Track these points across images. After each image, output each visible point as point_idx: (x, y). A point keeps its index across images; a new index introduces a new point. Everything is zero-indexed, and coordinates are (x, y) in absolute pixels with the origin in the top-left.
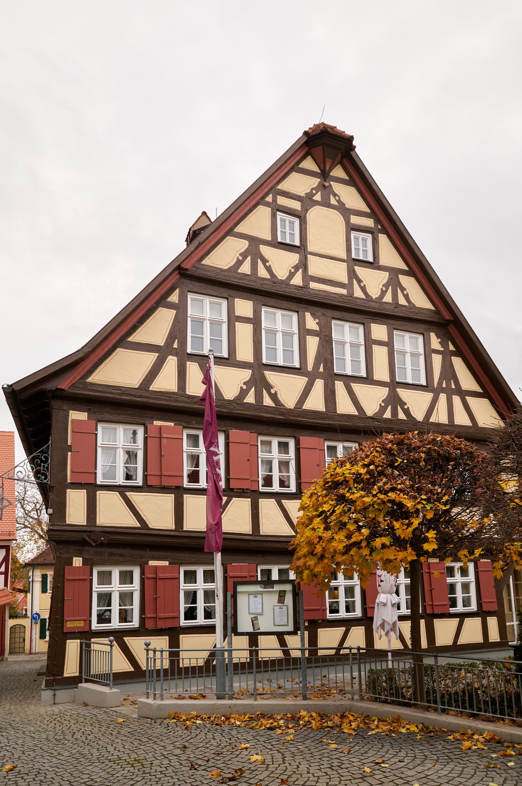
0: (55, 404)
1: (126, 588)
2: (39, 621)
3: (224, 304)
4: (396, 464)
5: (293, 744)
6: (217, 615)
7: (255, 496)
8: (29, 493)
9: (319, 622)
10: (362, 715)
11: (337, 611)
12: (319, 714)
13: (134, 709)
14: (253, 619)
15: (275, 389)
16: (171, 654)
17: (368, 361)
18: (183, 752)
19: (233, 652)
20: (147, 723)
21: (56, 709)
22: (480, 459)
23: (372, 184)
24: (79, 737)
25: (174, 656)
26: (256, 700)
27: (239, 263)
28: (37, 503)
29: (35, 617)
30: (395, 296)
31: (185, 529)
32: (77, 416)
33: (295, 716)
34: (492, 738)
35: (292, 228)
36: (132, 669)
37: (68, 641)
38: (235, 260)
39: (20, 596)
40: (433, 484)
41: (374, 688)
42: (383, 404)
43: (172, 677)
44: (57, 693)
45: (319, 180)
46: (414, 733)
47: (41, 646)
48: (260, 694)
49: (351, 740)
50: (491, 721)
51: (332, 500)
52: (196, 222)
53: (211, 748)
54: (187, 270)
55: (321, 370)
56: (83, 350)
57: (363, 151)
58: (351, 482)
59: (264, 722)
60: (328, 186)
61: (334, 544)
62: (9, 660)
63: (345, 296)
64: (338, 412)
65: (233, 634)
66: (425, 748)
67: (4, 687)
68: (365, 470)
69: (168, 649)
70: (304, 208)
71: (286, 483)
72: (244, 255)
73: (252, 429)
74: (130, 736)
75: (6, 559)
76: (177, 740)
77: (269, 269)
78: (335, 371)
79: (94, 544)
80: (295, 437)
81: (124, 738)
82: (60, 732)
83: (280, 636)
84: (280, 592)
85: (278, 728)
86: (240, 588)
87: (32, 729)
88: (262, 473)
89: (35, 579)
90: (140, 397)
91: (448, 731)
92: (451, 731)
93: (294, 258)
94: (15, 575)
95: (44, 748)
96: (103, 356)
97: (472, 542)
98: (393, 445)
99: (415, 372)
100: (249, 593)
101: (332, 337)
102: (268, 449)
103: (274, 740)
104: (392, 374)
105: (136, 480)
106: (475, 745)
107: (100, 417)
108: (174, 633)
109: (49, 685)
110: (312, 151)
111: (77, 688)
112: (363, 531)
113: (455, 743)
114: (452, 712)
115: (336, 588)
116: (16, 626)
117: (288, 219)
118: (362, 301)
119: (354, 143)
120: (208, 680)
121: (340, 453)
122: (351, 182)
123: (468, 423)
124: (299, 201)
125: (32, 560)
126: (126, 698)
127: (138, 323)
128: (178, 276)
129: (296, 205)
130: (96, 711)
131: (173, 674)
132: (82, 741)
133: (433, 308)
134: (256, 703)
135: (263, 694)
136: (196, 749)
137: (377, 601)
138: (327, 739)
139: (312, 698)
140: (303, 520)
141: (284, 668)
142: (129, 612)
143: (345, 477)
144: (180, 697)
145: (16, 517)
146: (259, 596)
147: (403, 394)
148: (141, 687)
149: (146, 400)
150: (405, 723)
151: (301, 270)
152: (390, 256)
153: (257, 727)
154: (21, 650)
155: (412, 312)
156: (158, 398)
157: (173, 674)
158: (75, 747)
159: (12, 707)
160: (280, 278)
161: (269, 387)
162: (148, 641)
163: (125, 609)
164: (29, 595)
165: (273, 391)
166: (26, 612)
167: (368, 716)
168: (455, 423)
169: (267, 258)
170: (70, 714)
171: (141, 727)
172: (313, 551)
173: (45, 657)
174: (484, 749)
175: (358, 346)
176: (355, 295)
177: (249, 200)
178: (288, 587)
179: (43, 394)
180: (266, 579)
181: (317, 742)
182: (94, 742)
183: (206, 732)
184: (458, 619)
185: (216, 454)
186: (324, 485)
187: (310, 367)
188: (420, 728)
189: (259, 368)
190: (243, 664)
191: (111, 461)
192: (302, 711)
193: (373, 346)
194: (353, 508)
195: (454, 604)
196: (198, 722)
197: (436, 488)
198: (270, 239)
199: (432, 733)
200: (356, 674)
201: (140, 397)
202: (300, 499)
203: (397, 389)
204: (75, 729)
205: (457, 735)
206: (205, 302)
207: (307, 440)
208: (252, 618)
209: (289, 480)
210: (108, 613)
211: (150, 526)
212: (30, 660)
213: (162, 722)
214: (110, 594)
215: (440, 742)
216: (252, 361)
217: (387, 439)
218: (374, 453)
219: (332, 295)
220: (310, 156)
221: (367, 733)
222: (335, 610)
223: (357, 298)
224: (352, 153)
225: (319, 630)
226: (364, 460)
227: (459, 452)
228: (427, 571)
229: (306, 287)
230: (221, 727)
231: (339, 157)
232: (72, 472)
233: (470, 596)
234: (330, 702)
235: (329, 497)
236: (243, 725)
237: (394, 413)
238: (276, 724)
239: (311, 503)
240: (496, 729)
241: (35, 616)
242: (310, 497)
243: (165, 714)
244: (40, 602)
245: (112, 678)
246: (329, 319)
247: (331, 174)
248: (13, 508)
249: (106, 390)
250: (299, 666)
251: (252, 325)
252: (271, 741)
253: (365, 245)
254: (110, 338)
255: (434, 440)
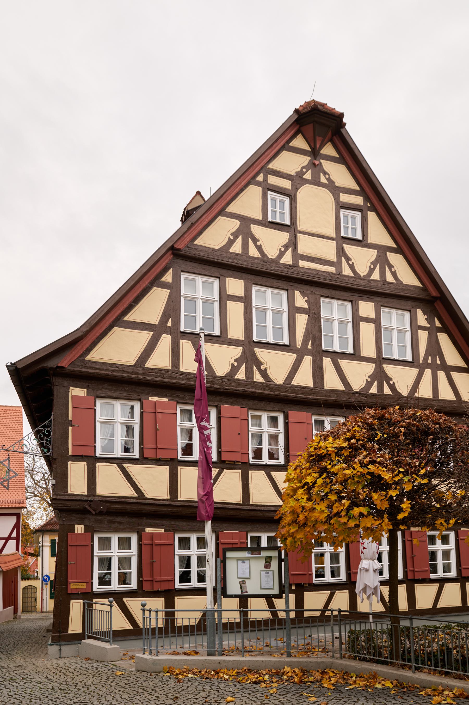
0: (56, 381)
1: (125, 553)
2: (49, 583)
3: (216, 283)
4: (376, 439)
5: (275, 697)
6: (208, 579)
7: (245, 468)
8: (38, 464)
9: (305, 586)
10: (341, 671)
11: (323, 576)
12: (302, 670)
13: (132, 664)
14: (241, 583)
15: (265, 365)
16: (167, 614)
17: (356, 337)
18: (174, 702)
19: (223, 612)
20: (143, 676)
21: (61, 662)
22: (458, 433)
23: (361, 161)
24: (81, 688)
25: (170, 616)
26: (243, 657)
27: (231, 243)
28: (45, 473)
29: (45, 580)
30: (383, 273)
31: (179, 499)
32: (77, 392)
33: (279, 672)
34: (461, 694)
35: (282, 207)
36: (131, 628)
37: (72, 601)
38: (227, 239)
39: (32, 560)
40: (412, 457)
41: (353, 646)
42: (369, 380)
43: (167, 635)
44: (63, 648)
45: (310, 158)
46: (388, 688)
47: (49, 605)
48: (249, 651)
49: (330, 694)
50: (462, 679)
51: (315, 473)
52: (191, 202)
53: (201, 699)
54: (180, 250)
55: (310, 346)
56: (81, 329)
57: (354, 129)
58: (333, 455)
59: (250, 676)
60: (318, 165)
61: (316, 514)
62: (22, 617)
63: (334, 274)
64: (325, 388)
65: (222, 597)
66: (397, 702)
67: (16, 642)
68: (347, 444)
69: (164, 609)
70: (295, 187)
71: (275, 456)
72: (236, 235)
73: (243, 404)
74: (128, 687)
75: (17, 526)
76: (170, 691)
77: (259, 248)
78: (323, 348)
79: (94, 513)
80: (284, 412)
81: (122, 689)
82: (64, 683)
83: (269, 598)
84: (267, 558)
85: (263, 682)
86: (229, 554)
87: (39, 680)
88: (252, 446)
89: (45, 544)
90: (136, 374)
91: (421, 687)
92: (424, 687)
93: (284, 237)
94: (27, 541)
95: (49, 696)
96: (100, 335)
97: (447, 511)
98: (374, 420)
99: (402, 348)
100: (238, 559)
101: (320, 315)
102: (258, 423)
103: (258, 692)
104: (382, 351)
105: (133, 453)
106: (444, 700)
107: (98, 393)
108: (169, 595)
109: (55, 641)
110: (303, 129)
111: (80, 644)
112: (344, 501)
113: (426, 698)
114: (425, 670)
115: (322, 555)
116: (28, 587)
117: (278, 198)
118: (350, 279)
119: (344, 120)
120: (199, 639)
121: (327, 426)
122: (341, 160)
123: (452, 397)
124: (289, 179)
125: (42, 526)
126: (126, 653)
127: (133, 302)
128: (172, 256)
129: (286, 184)
130: (97, 665)
131: (167, 632)
132: (84, 691)
133: (420, 285)
134: (243, 659)
135: (252, 651)
136: (187, 700)
137: (360, 567)
138: (307, 693)
139: (297, 655)
140: (288, 492)
141: (263, 628)
142: (128, 576)
143: (328, 451)
144: (175, 653)
145: (26, 486)
146: (247, 562)
147: (389, 369)
148: (138, 644)
149: (141, 377)
150: (381, 679)
151: (290, 249)
152: (378, 234)
153: (243, 681)
154: (34, 608)
155: (399, 289)
156: (153, 375)
157: (167, 632)
158: (77, 696)
159: (22, 660)
160: (270, 257)
161: (259, 364)
162: (144, 602)
163: (124, 573)
164: (40, 559)
165: (263, 368)
166: (37, 574)
167: (347, 672)
168: (440, 398)
169: (257, 237)
170: (74, 667)
171: (138, 679)
172: (297, 520)
173: (52, 615)
174: (453, 704)
175: (346, 323)
176: (344, 273)
177: (240, 180)
178: (274, 554)
179: (45, 371)
180: (256, 546)
181: (298, 695)
182: (94, 692)
183: (197, 685)
184: (438, 584)
185: (207, 429)
186: (309, 458)
187: (299, 344)
188: (394, 684)
189: (249, 345)
190: (232, 624)
191: (109, 435)
192: (286, 667)
193: (361, 323)
194: (334, 480)
195: (434, 570)
196: (190, 675)
197: (414, 461)
198: (261, 218)
199: (405, 689)
200: (337, 634)
201: (136, 374)
202: (287, 471)
203: (384, 365)
204: (78, 680)
205: (429, 691)
206: (197, 281)
207: (295, 415)
208: (240, 582)
209: (278, 453)
210: (109, 576)
211: (147, 496)
212: (41, 618)
213: (157, 675)
214: (110, 559)
215: (413, 697)
216: (243, 339)
217: (368, 414)
218: (356, 428)
219: (321, 273)
220: (300, 134)
221: (345, 688)
222: (320, 575)
223: (345, 276)
224: (342, 130)
225: (305, 593)
226: (345, 434)
227: (438, 426)
228: (409, 539)
229: (295, 265)
230: (211, 680)
231: (330, 134)
232: (73, 445)
233: (450, 563)
234: (312, 659)
235: (312, 469)
236: (231, 679)
237: (380, 388)
238: (261, 678)
239: (296, 475)
240: (465, 686)
241: (45, 578)
242: (295, 469)
243: (160, 668)
244: (47, 565)
245: (112, 635)
246: (318, 297)
247: (322, 152)
248: (23, 478)
249: (103, 367)
250: (283, 627)
251: (243, 304)
252: (256, 693)
253: (354, 223)
254: (107, 318)
255: (413, 414)
